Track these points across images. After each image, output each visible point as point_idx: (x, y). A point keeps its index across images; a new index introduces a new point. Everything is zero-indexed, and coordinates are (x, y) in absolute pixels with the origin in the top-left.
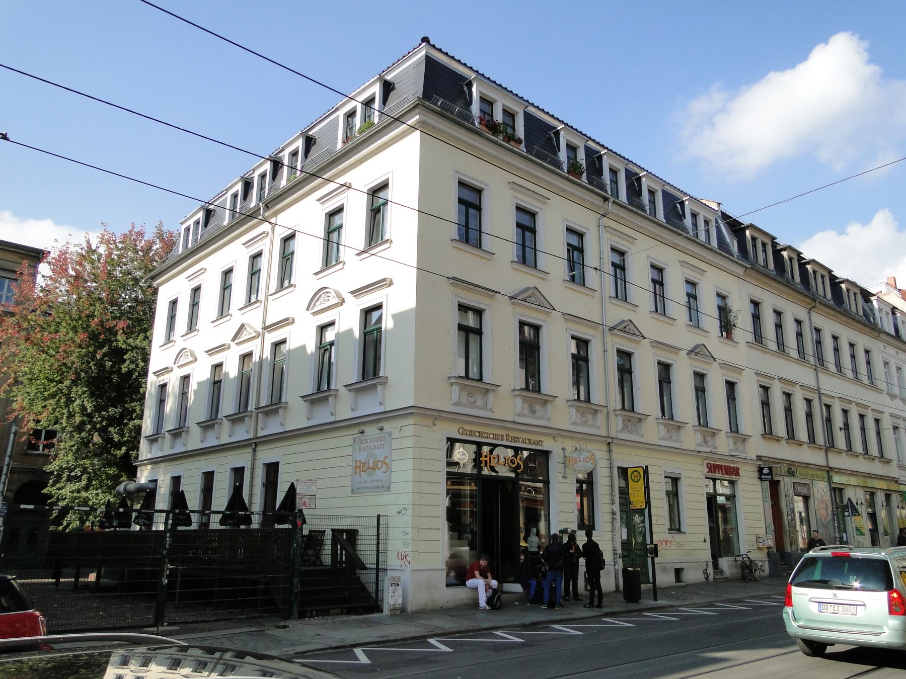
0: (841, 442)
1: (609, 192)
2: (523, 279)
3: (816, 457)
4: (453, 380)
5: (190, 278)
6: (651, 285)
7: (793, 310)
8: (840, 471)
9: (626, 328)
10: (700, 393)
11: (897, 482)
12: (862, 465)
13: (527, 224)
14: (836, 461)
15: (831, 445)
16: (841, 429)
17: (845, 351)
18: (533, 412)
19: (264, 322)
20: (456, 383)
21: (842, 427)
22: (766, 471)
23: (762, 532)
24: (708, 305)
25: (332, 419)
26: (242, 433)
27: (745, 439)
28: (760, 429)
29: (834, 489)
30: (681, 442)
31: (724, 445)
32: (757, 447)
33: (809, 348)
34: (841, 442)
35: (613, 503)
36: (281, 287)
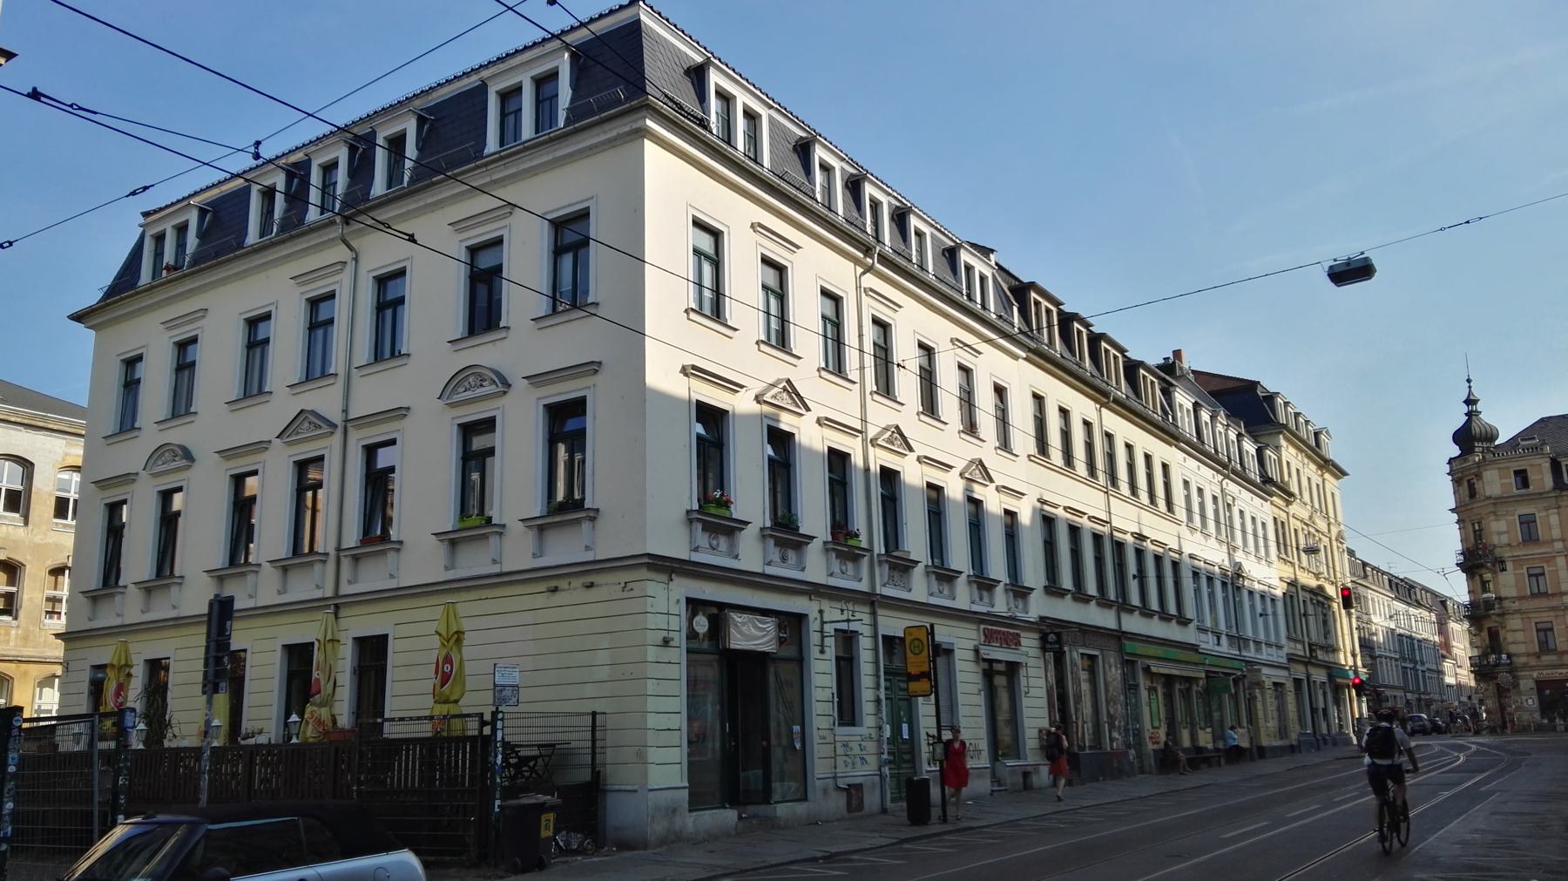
2: (772, 367)
5: (169, 324)
6: (761, 294)
8: (1134, 637)
12: (1156, 628)
18: (784, 559)
19: (345, 411)
20: (699, 520)
22: (1052, 637)
24: (806, 312)
25: (496, 569)
26: (304, 587)
30: (803, 569)
31: (1001, 603)
32: (1039, 606)
33: (1054, 438)
35: (878, 687)
36: (378, 357)
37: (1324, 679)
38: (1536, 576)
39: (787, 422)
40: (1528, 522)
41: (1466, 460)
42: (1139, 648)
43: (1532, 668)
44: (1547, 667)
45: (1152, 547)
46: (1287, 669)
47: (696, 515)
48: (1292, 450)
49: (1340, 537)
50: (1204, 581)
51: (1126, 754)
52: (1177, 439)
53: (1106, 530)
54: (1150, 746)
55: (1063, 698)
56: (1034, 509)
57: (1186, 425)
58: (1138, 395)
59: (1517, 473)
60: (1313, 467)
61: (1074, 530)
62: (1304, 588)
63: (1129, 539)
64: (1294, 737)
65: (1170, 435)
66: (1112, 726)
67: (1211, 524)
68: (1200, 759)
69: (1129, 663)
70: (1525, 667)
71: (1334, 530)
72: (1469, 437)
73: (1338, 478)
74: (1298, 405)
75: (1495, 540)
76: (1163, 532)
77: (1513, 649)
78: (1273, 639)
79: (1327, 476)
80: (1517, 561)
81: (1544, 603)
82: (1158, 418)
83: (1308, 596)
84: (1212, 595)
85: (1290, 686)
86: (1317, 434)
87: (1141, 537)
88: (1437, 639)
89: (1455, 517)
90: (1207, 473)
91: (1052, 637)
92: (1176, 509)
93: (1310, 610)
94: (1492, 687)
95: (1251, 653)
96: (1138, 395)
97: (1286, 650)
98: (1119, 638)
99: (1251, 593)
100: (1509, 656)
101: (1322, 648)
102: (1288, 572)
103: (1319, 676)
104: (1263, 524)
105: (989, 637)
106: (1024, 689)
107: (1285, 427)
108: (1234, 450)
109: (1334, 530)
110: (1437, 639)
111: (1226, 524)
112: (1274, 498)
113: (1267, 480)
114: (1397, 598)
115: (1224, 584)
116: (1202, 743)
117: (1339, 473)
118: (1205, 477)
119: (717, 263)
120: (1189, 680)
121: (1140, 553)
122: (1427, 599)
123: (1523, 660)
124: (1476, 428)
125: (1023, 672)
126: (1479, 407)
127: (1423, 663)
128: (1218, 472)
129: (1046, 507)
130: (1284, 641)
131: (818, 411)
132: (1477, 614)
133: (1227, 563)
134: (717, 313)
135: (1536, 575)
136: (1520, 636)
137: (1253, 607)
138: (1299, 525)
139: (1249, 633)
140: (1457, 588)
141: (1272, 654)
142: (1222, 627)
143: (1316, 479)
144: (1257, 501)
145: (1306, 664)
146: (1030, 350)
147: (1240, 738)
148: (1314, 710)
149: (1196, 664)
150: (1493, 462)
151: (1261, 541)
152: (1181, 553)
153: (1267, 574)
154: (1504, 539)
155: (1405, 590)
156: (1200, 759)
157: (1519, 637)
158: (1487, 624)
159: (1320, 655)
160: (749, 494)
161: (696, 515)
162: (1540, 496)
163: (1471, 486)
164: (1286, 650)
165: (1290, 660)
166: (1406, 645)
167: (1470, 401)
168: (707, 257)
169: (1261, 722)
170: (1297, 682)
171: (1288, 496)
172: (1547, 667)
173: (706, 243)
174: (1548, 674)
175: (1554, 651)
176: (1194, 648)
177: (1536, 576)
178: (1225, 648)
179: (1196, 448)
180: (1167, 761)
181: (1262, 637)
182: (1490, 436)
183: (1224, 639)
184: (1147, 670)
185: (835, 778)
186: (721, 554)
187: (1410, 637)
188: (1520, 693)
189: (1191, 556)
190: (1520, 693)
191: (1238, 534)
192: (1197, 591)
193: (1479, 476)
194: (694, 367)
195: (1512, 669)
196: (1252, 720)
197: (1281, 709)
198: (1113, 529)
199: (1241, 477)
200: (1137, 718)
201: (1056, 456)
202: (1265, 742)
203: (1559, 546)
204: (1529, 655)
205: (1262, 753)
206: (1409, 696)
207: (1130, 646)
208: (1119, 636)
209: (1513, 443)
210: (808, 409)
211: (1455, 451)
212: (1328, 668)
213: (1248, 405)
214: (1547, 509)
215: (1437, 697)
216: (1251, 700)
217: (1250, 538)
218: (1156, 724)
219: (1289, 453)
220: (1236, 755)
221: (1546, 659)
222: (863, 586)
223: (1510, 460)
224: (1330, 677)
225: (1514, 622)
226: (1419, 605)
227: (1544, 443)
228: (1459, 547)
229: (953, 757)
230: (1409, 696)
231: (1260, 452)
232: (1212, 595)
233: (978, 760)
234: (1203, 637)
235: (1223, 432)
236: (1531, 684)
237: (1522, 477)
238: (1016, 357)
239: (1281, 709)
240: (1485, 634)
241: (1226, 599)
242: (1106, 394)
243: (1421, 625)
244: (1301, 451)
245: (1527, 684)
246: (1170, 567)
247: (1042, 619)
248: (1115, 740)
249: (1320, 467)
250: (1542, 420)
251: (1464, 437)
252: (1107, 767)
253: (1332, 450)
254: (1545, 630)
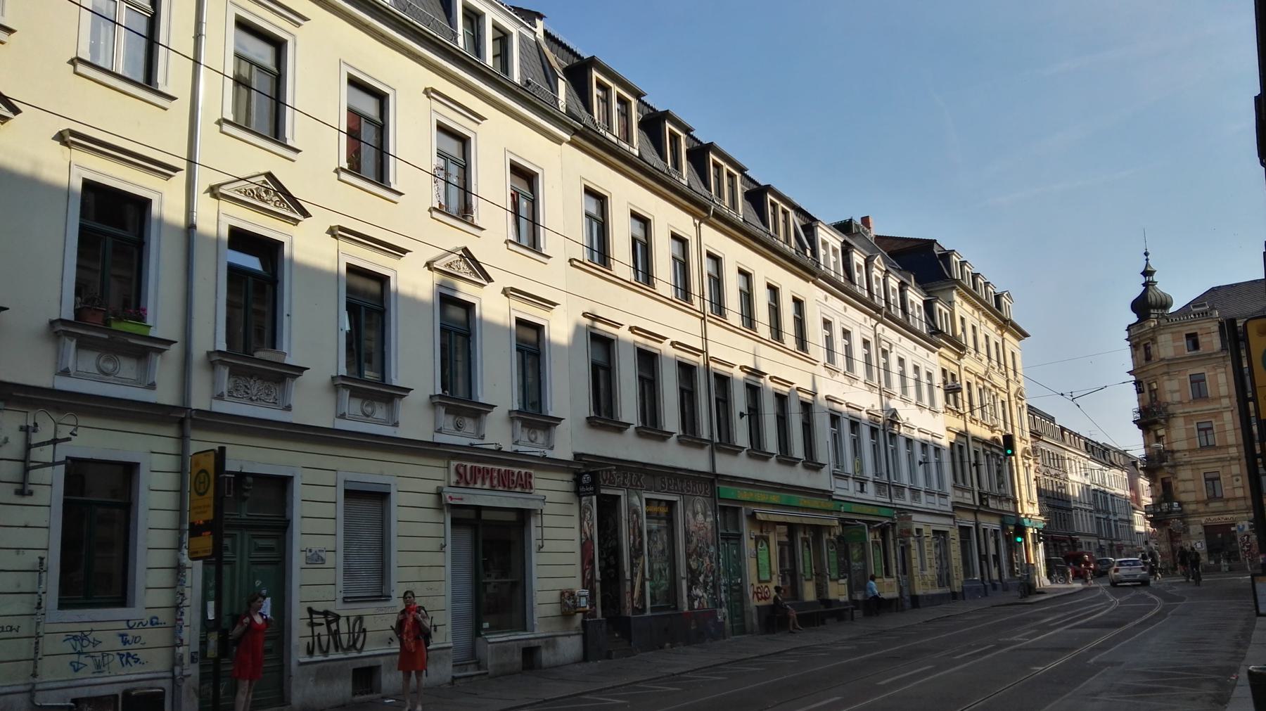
0: (741, 436)
1: (616, 132)
3: (697, 461)
4: (60, 328)
7: (669, 218)
8: (734, 481)
9: (277, 194)
10: (529, 361)
11: (830, 497)
12: (772, 472)
13: (457, 149)
14: (727, 465)
15: (725, 444)
16: (742, 415)
17: (910, 373)
21: (745, 411)
22: (586, 478)
23: (576, 585)
24: (492, 185)
27: (285, 375)
28: (585, 407)
29: (724, 509)
30: (552, 448)
32: (571, 439)
34: (741, 436)
37: (997, 526)
38: (1205, 430)
39: (466, 291)
40: (1197, 381)
41: (1142, 326)
42: (744, 494)
43: (1200, 514)
44: (1214, 513)
45: (771, 385)
46: (950, 516)
47: (437, 400)
48: (966, 306)
49: (1020, 395)
50: (846, 426)
51: (712, 614)
52: (814, 274)
53: (699, 360)
54: (754, 603)
55: (611, 553)
56: (578, 327)
57: (831, 261)
58: (764, 221)
59: (1188, 336)
60: (992, 326)
61: (647, 359)
62: (975, 439)
63: (738, 374)
64: (957, 584)
65: (809, 271)
66: (693, 582)
67: (860, 368)
68: (825, 613)
69: (729, 512)
70: (1195, 513)
71: (1013, 388)
72: (1147, 306)
73: (1019, 339)
74: (975, 266)
75: (1168, 398)
76: (783, 369)
77: (1183, 497)
78: (935, 487)
79: (1006, 335)
80: (1188, 417)
81: (1213, 455)
82: (792, 248)
83: (981, 447)
84: (856, 443)
85: (954, 534)
86: (998, 298)
87: (757, 373)
88: (1128, 493)
89: (1133, 378)
90: (859, 316)
91: (586, 478)
92: (811, 347)
93: (982, 459)
94: (1165, 532)
95: (907, 501)
96: (764, 221)
97: (950, 499)
98: (712, 482)
99: (909, 441)
100: (1180, 504)
101: (995, 497)
102: (958, 424)
103: (992, 524)
104: (929, 375)
105: (464, 480)
106: (534, 544)
107: (957, 281)
108: (895, 298)
109: (1013, 388)
110: (1128, 493)
111: (877, 364)
112: (942, 350)
113: (935, 331)
114: (1092, 459)
115: (874, 431)
116: (832, 595)
117: (1021, 334)
118: (859, 323)
119: (465, 169)
120: (817, 530)
121: (754, 391)
122: (1120, 460)
123: (1193, 507)
124: (1152, 297)
125: (534, 522)
126: (1155, 277)
127: (1115, 514)
128: (871, 316)
129: (599, 325)
130: (948, 488)
131: (501, 281)
132: (1154, 465)
133: (878, 407)
134: (534, 246)
135: (1205, 430)
136: (1190, 486)
137: (911, 456)
138: (973, 379)
139: (905, 480)
140: (1134, 443)
141: (932, 505)
142: (869, 472)
143: (995, 337)
144: (922, 351)
145: (975, 512)
146: (576, 132)
147: (885, 588)
148: (983, 558)
149: (831, 512)
150: (1166, 327)
151: (925, 389)
152: (814, 394)
153: (930, 423)
154: (1177, 397)
155: (1100, 453)
156: (825, 613)
157: (1189, 486)
158: (1161, 475)
159: (992, 504)
160: (497, 381)
161: (437, 400)
162: (1209, 357)
163: (1147, 348)
164: (950, 499)
165: (954, 508)
166: (1099, 497)
167: (1147, 273)
168: (369, 120)
169: (916, 571)
170: (965, 531)
171: (959, 348)
172: (1214, 513)
173: (453, 147)
174: (1215, 519)
175: (1221, 499)
176: (826, 494)
177: (1205, 430)
178: (871, 493)
179: (844, 289)
180: (774, 619)
181: (921, 484)
182: (1165, 304)
183: (870, 487)
184: (752, 517)
185: (32, 692)
186: (378, 422)
187: (1104, 492)
188: (1189, 538)
189: (828, 398)
190: (1189, 538)
191: (896, 380)
192: (836, 438)
193: (1154, 340)
194: (341, 229)
195: (1183, 516)
196: (906, 568)
197: (944, 557)
198: (709, 359)
199: (904, 327)
200: (740, 572)
201: (764, 330)
202: (919, 591)
203: (1225, 402)
204: (1197, 502)
205: (916, 601)
206: (1102, 542)
207: (727, 491)
208: (712, 480)
209: (1185, 310)
210: (489, 279)
211: (1134, 318)
212: (1002, 516)
213: (924, 263)
214: (1214, 368)
215: (1127, 542)
216: (905, 549)
217: (911, 383)
218: (765, 576)
219: (963, 309)
220: (877, 606)
221: (1215, 505)
222: (165, 394)
223: (1182, 324)
224: (1004, 526)
225: (1185, 473)
226: (1112, 465)
227: (1212, 308)
228: (1136, 405)
229: (413, 630)
230: (1102, 542)
231: (928, 306)
232: (856, 443)
233: (442, 638)
234: (841, 483)
235: (884, 279)
236: (1200, 529)
237: (1193, 340)
238: (559, 141)
239: (944, 557)
240: (1159, 484)
241: (875, 448)
242: (705, 208)
243: (1115, 482)
244: (979, 309)
245: (1196, 529)
246: (796, 412)
247: (578, 456)
248: (695, 598)
249: (1000, 327)
250: (1213, 289)
251: (1142, 306)
252: (676, 628)
253: (1013, 312)
254: (1213, 480)
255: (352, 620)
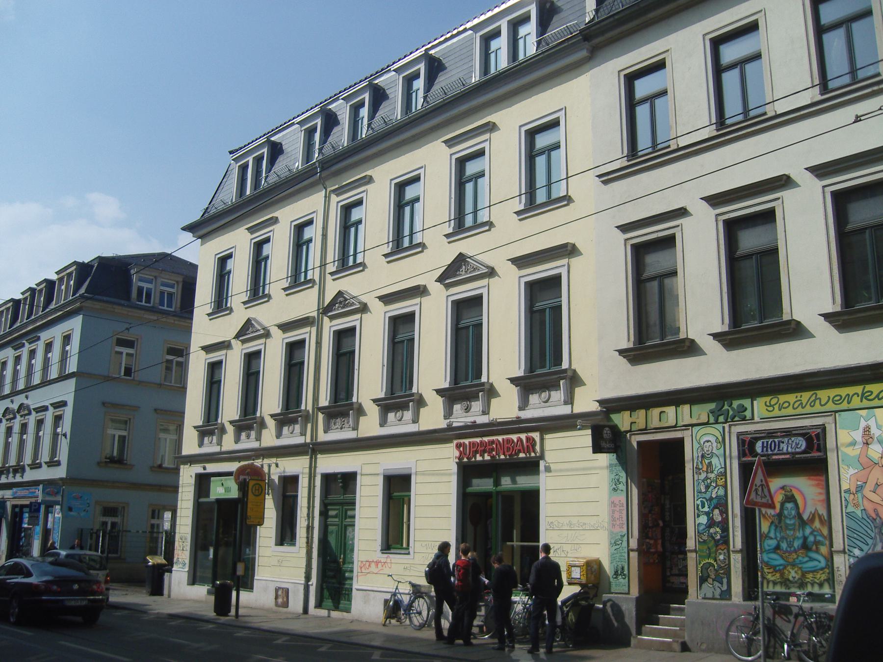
255: (548, 527)
